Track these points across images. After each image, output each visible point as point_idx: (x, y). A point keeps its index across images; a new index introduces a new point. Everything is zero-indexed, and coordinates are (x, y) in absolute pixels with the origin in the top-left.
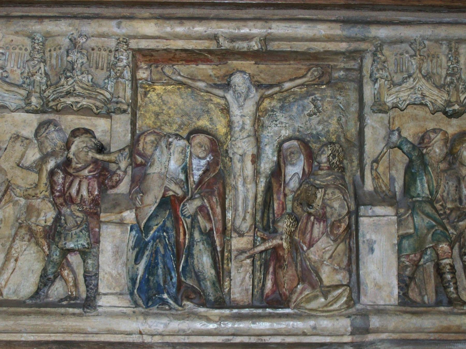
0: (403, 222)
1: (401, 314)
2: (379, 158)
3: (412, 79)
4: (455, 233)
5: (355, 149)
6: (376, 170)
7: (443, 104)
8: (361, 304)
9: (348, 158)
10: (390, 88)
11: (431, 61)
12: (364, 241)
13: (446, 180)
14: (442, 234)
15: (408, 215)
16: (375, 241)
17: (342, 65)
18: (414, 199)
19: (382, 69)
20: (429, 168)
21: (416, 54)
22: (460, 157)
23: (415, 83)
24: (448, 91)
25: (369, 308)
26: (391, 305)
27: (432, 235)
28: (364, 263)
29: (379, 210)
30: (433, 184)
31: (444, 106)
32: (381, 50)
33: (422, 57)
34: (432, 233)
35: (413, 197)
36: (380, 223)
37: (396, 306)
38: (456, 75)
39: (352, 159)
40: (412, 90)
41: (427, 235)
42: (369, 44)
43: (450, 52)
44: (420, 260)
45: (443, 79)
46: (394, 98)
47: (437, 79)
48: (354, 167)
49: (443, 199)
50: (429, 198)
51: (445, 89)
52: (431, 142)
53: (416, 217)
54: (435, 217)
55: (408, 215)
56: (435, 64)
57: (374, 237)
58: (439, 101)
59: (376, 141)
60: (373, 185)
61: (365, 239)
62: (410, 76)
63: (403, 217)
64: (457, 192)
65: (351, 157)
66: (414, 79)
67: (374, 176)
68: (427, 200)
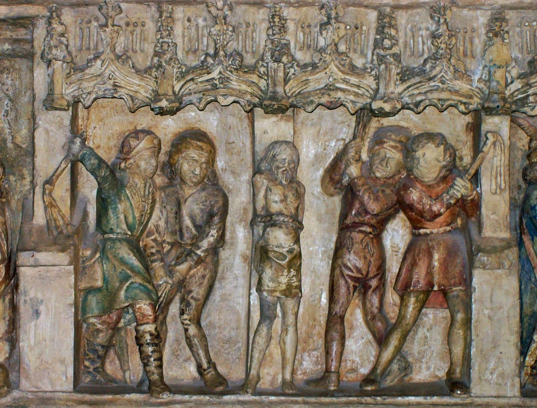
0: (87, 270)
1: (74, 404)
2: (54, 177)
3: (99, 62)
4: (170, 282)
5: (28, 159)
6: (50, 194)
7: (150, 97)
8: (20, 391)
9: (17, 173)
10: (69, 73)
11: (132, 33)
12: (25, 301)
13: (163, 202)
14: (142, 288)
15: (94, 259)
16: (42, 301)
17: (9, 34)
18: (106, 236)
19: (56, 47)
20: (127, 192)
21: (107, 22)
22: (179, 171)
23: (103, 68)
24: (156, 78)
25: (30, 396)
26: (63, 392)
27: (126, 291)
28: (25, 332)
29: (43, 257)
30: (133, 214)
31: (150, 99)
32: (58, 16)
33: (116, 28)
34: (125, 287)
35: (106, 233)
36: (49, 274)
37: (70, 392)
38: (165, 54)
39: (23, 175)
40: (99, 79)
41: (119, 289)
42: (41, 7)
43: (160, 19)
44: (118, 321)
45: (150, 59)
46: (75, 89)
47: (140, 60)
48: (25, 186)
49: (157, 231)
50: (127, 234)
51: (151, 75)
52: (132, 151)
53: (105, 263)
54: (132, 264)
55: (94, 259)
56: (139, 36)
57: (40, 296)
58: (142, 91)
59: (50, 150)
60: (46, 217)
61: (27, 298)
62: (96, 57)
63: (88, 264)
64: (178, 220)
65: (21, 170)
66: (103, 62)
67: (47, 203)
68: (124, 237)
